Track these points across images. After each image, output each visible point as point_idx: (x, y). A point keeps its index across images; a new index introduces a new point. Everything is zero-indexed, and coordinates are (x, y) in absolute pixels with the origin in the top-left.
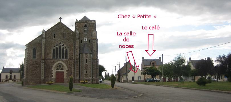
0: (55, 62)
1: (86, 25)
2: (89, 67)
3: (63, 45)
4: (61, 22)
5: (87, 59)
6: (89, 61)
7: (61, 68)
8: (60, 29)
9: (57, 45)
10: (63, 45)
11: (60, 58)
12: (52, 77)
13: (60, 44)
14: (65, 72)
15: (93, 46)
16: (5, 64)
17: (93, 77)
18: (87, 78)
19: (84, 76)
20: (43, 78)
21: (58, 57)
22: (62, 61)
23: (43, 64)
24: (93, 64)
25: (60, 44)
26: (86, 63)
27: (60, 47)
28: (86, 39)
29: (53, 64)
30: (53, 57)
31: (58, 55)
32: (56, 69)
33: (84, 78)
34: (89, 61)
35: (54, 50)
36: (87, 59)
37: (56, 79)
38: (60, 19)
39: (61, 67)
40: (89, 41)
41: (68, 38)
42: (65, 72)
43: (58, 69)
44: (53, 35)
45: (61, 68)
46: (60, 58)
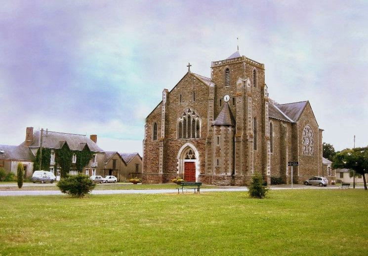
0: (182, 145)
1: (227, 69)
2: (222, 152)
3: (194, 114)
4: (192, 75)
5: (219, 136)
6: (224, 139)
7: (191, 155)
8: (189, 84)
9: (185, 114)
10: (194, 114)
11: (189, 137)
12: (178, 172)
13: (189, 111)
14: (197, 162)
15: (238, 110)
16: (363, 189)
17: (236, 174)
18: (220, 175)
19: (215, 169)
20: (162, 173)
21: (187, 136)
22: (191, 142)
23: (161, 149)
24: (235, 146)
25: (189, 111)
26: (218, 145)
27: (189, 117)
28: (227, 98)
29: (180, 147)
30: (180, 137)
31: (187, 133)
32: (185, 157)
33: (215, 174)
34: (224, 139)
35: (180, 123)
36: (219, 136)
37: (90, 159)
38: (189, 66)
39: (191, 154)
40: (234, 99)
41: (200, 100)
42: (197, 162)
43: (187, 158)
44: (179, 97)
45: (191, 155)
46: (189, 137)
